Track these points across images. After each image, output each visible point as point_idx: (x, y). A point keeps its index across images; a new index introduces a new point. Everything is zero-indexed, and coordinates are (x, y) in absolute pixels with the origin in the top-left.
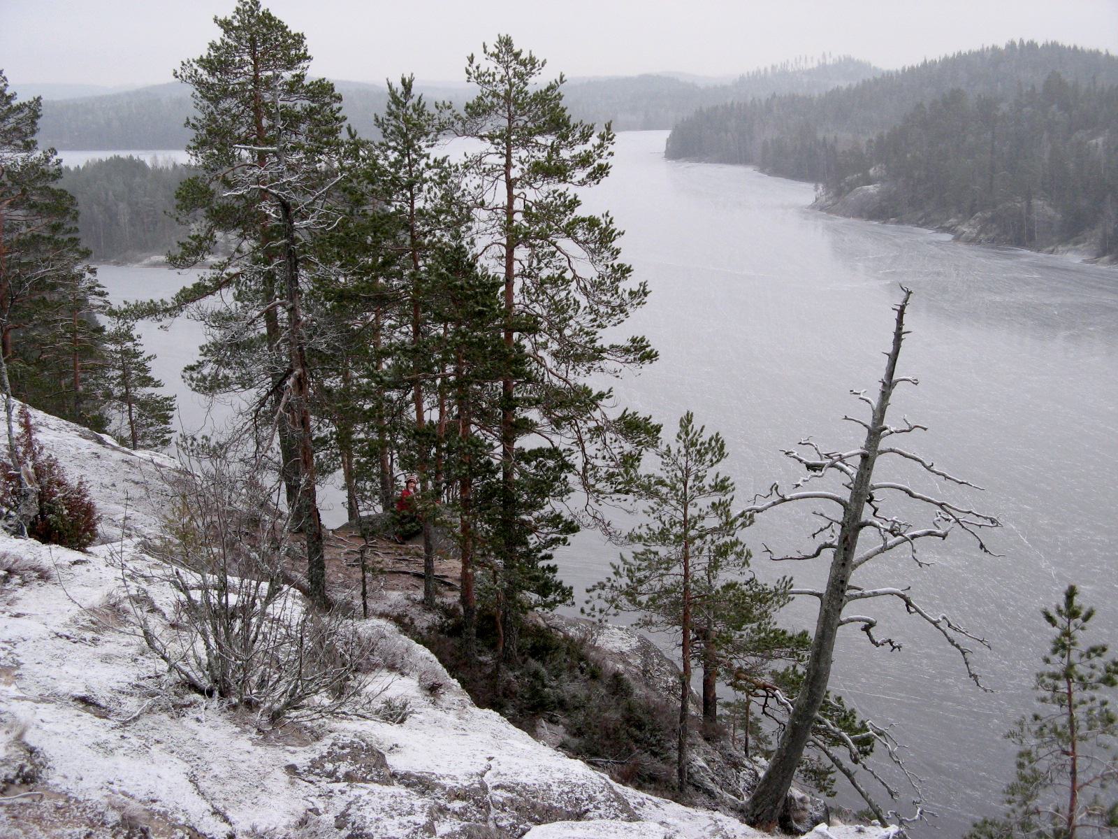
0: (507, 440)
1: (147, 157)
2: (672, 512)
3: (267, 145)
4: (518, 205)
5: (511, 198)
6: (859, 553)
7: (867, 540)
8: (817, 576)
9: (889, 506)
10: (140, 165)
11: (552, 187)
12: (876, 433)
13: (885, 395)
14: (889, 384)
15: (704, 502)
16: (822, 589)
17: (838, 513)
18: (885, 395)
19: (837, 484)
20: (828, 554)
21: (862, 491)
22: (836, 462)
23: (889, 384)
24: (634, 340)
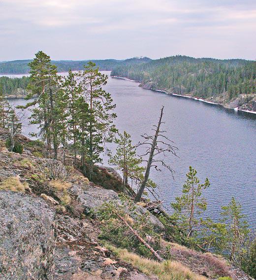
0: (91, 133)
1: (11, 76)
2: (122, 146)
3: (18, 80)
4: (93, 90)
5: (91, 88)
6: (154, 153)
7: (156, 151)
8: (147, 157)
9: (159, 145)
10: (8, 78)
11: (109, 173)
12: (158, 131)
13: (159, 125)
14: (160, 123)
15: (127, 145)
16: (148, 160)
17: (151, 146)
18: (159, 125)
19: (151, 141)
20: (149, 154)
21: (155, 143)
22: (151, 137)
23: (160, 123)
24: (106, 82)
